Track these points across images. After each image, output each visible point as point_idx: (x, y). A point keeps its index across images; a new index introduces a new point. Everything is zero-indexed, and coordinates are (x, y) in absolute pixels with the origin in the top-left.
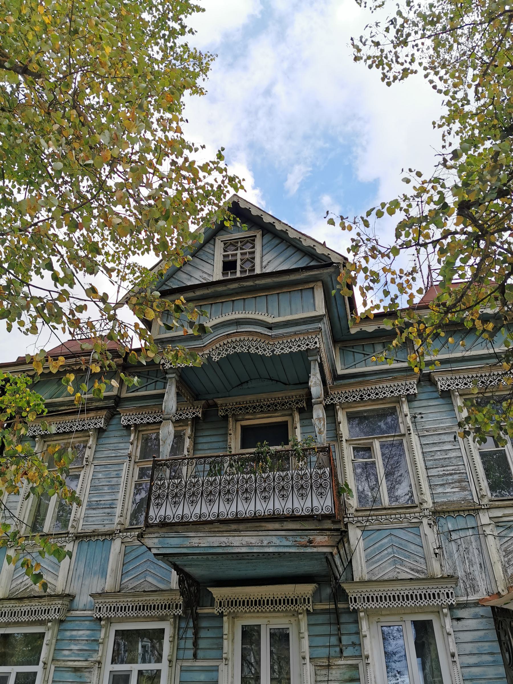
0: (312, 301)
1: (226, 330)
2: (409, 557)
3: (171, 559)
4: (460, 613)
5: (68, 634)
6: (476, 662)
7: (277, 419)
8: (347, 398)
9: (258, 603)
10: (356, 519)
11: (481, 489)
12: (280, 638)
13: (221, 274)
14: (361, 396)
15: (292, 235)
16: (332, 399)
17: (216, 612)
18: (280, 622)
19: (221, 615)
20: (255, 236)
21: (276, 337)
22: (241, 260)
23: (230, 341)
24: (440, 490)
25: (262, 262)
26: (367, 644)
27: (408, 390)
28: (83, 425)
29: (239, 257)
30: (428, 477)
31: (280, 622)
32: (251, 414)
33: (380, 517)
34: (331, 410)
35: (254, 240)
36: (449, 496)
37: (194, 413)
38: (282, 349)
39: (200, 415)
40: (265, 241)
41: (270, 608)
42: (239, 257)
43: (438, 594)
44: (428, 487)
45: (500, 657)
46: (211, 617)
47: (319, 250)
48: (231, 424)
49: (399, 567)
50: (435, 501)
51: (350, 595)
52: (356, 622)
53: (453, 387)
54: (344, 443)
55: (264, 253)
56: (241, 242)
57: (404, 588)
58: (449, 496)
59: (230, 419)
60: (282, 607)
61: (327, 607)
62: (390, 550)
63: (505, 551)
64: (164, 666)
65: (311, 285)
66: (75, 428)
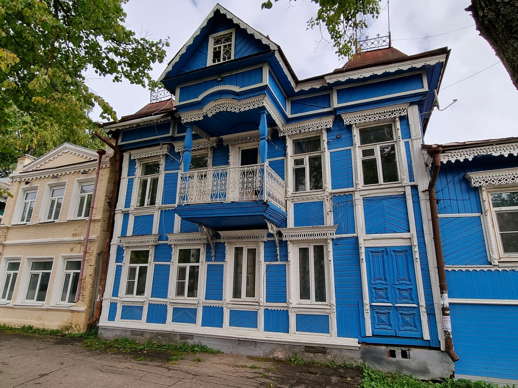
8: (500, 181)
9: (241, 238)
12: (252, 253)
19: (225, 243)
22: (224, 50)
27: (326, 126)
29: (222, 48)
42: (222, 48)
53: (353, 122)
54: (357, 147)
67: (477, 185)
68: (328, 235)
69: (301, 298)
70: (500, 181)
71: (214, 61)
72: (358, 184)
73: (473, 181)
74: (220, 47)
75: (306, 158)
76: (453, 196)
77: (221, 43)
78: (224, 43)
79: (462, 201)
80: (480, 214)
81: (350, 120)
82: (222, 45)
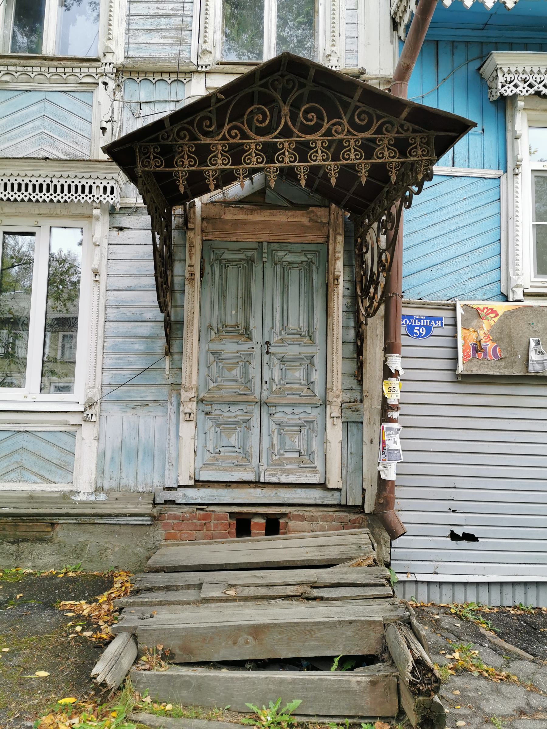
2: (66, 136)
4: (124, 221)
6: (130, 285)
11: (205, 42)
24: (143, 38)
30: (129, 15)
33: (30, 69)
36: (154, 50)
43: (91, 187)
44: (123, 31)
49: (47, 149)
50: (130, 55)
57: (37, 174)
58: (154, 50)
62: (38, 123)
67: (508, 91)
73: (501, 79)
80: (500, 173)
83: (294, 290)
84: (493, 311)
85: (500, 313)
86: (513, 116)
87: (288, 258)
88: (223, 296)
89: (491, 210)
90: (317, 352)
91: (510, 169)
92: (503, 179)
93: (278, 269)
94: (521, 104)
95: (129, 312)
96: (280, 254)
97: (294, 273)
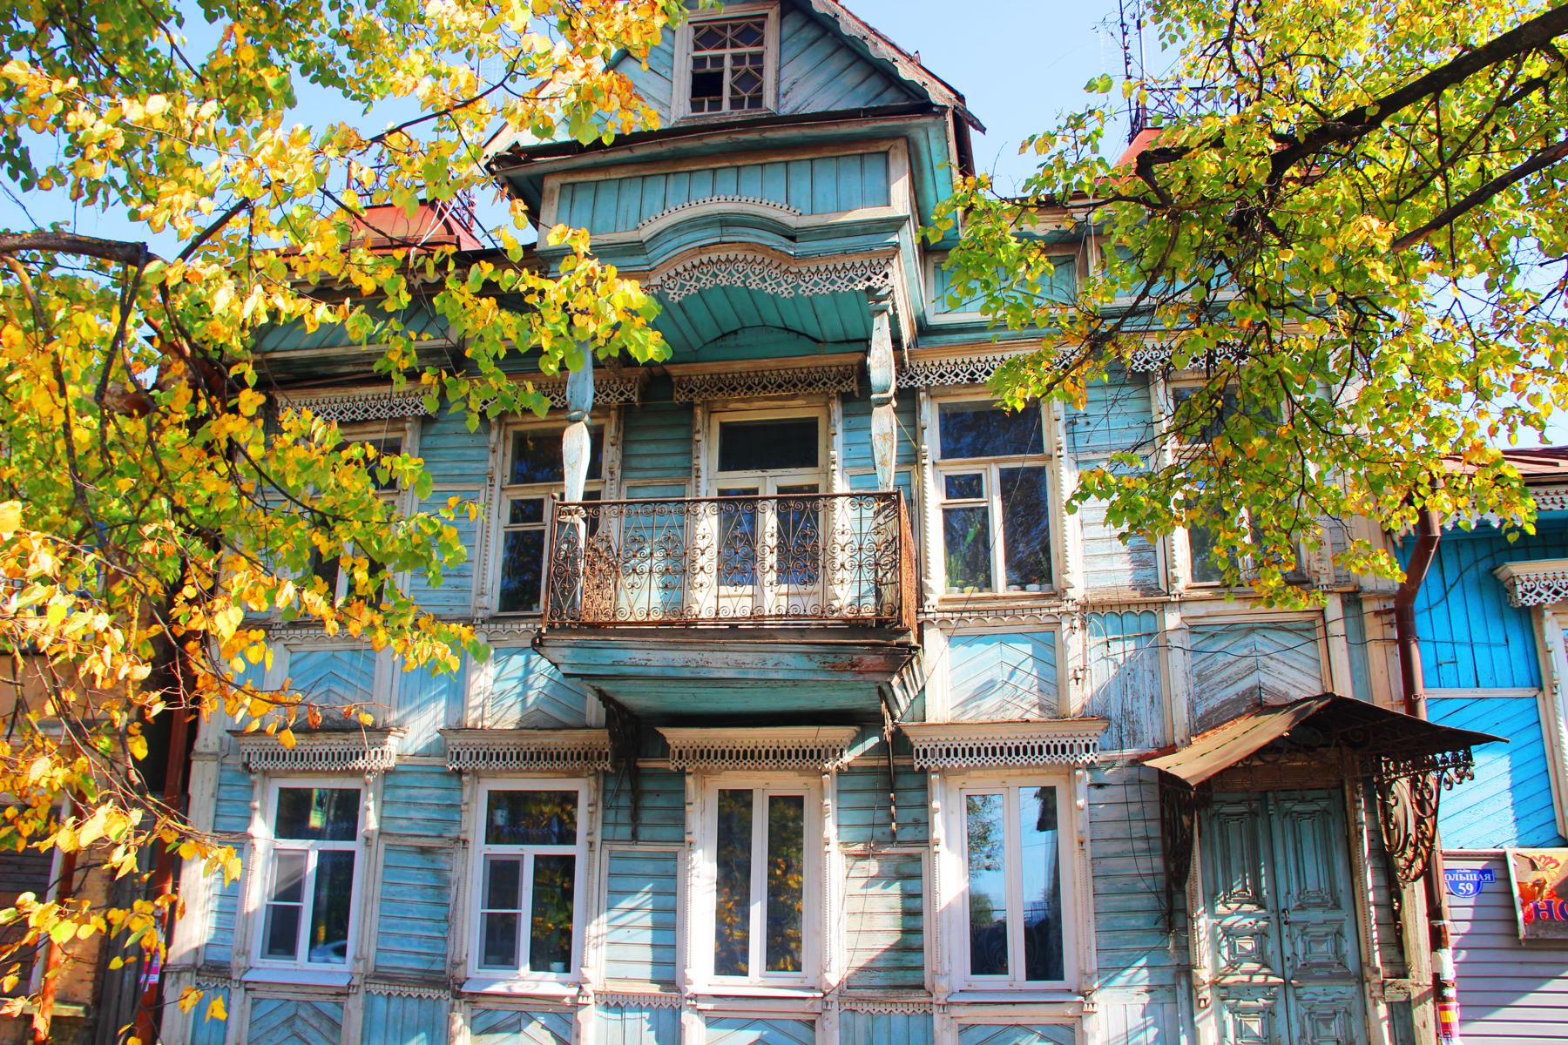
0: (883, 183)
1: (698, 235)
3: (596, 684)
5: (402, 793)
7: (796, 410)
8: (942, 376)
10: (939, 615)
13: (688, 104)
14: (972, 374)
15: (848, 28)
16: (911, 378)
17: (672, 768)
18: (786, 782)
19: (682, 773)
20: (766, 16)
21: (804, 257)
22: (734, 72)
23: (705, 260)
25: (778, 82)
26: (938, 821)
28: (391, 409)
29: (728, 63)
31: (786, 782)
32: (743, 400)
34: (907, 400)
35: (761, 25)
37: (622, 394)
38: (816, 284)
39: (635, 398)
40: (787, 31)
41: (771, 762)
42: (728, 63)
45: (1158, 844)
46: (667, 774)
47: (906, 72)
48: (699, 418)
51: (916, 746)
52: (924, 787)
55: (784, 61)
56: (733, 27)
59: (699, 411)
60: (793, 763)
61: (874, 763)
63: (1198, 676)
64: (577, 850)
65: (883, 147)
66: (372, 414)
67: (1531, 601)
68: (1076, 751)
69: (974, 972)
70: (942, 376)
71: (696, 106)
72: (1176, 579)
73: (1520, 589)
74: (718, 60)
75: (991, 472)
76: (1460, 633)
77: (723, 46)
78: (734, 45)
79: (1486, 650)
80: (1534, 692)
81: (1147, 357)
82: (728, 53)
83: (1308, 845)
84: (1552, 860)
85: (1562, 862)
86: (1540, 624)
87: (1298, 808)
88: (1226, 859)
89: (1532, 735)
90: (1344, 914)
91: (1545, 687)
92: (1540, 697)
93: (1287, 821)
94: (1547, 614)
95: (1120, 883)
96: (1288, 805)
97: (1306, 825)
